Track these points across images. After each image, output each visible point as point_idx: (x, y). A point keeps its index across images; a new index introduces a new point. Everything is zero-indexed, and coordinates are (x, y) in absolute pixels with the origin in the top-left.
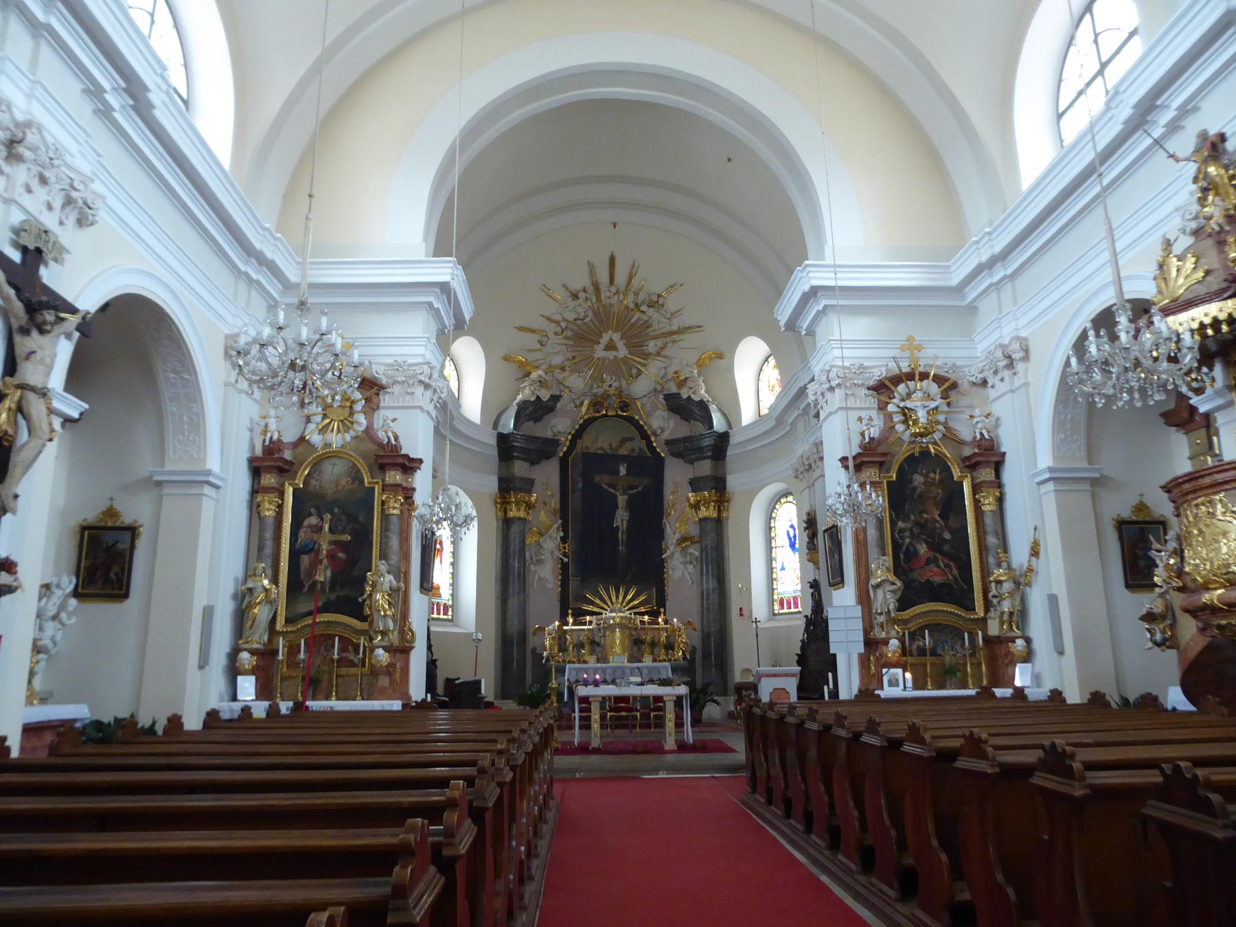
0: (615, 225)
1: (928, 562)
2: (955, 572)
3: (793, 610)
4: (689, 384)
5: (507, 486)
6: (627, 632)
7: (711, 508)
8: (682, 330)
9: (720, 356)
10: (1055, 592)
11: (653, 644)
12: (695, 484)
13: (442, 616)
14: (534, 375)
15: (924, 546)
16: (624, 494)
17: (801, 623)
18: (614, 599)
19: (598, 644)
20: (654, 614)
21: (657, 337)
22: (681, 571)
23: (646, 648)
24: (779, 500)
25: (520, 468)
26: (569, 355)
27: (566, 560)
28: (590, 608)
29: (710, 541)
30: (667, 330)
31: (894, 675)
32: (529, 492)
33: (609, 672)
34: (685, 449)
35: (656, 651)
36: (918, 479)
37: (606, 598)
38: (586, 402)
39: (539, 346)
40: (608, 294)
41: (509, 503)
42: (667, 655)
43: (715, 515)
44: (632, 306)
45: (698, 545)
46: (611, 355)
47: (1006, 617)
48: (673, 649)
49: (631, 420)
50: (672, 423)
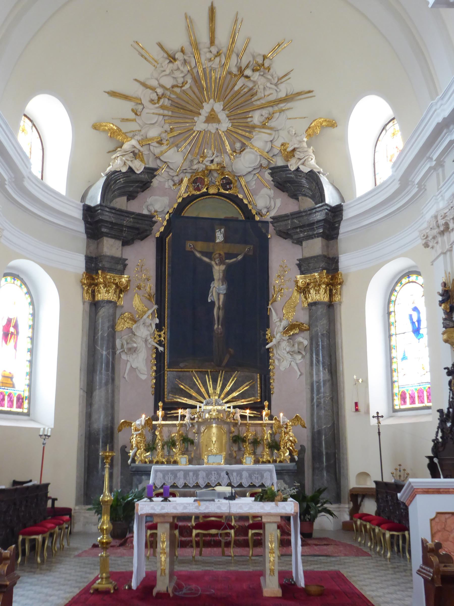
3: (417, 405)
4: (298, 155)
5: (94, 265)
6: (225, 428)
7: (322, 291)
8: (288, 99)
9: (332, 124)
11: (256, 443)
12: (304, 266)
13: (14, 409)
14: (127, 146)
17: (433, 420)
18: (211, 390)
19: (192, 442)
20: (257, 407)
21: (262, 107)
22: (288, 361)
23: (248, 447)
24: (399, 281)
25: (110, 247)
26: (167, 127)
27: (161, 349)
28: (185, 400)
29: (321, 327)
30: (273, 97)
32: (122, 272)
33: (202, 475)
34: (294, 229)
35: (259, 450)
37: (203, 390)
38: (185, 180)
39: (133, 116)
40: (209, 55)
41: (97, 285)
42: (272, 454)
43: (326, 299)
44: (235, 70)
45: (307, 334)
46: (212, 127)
48: (278, 449)
49: (234, 199)
50: (279, 202)
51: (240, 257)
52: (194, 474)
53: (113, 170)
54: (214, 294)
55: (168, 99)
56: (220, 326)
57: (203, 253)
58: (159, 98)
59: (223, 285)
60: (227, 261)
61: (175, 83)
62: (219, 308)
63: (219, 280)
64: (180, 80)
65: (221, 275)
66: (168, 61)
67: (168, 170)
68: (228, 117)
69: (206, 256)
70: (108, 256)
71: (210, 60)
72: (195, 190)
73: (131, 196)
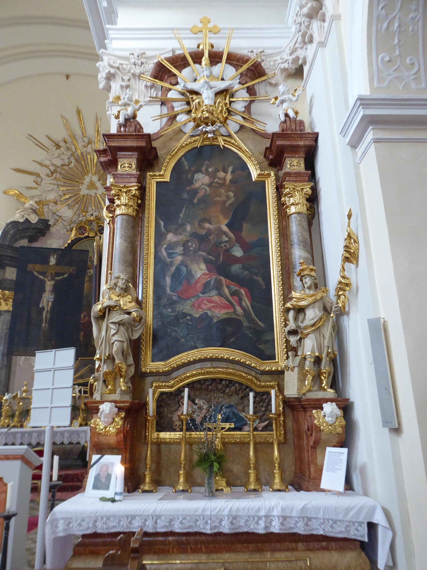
0: (68, 77)
1: (206, 288)
2: (246, 302)
10: (382, 315)
15: (203, 266)
16: (52, 279)
31: (107, 466)
36: (201, 180)
39: (35, 185)
40: (82, 144)
46: (92, 192)
47: (308, 365)
51: (66, 276)
52: (61, 435)
53: (12, 221)
54: (45, 301)
55: (60, 174)
56: (47, 325)
57: (39, 272)
58: (52, 173)
59: (51, 295)
60: (56, 278)
61: (63, 163)
62: (47, 311)
63: (49, 292)
64: (67, 161)
65: (51, 288)
66: (56, 148)
67: (62, 221)
68: (102, 185)
69: (42, 275)
70: (9, 280)
71: (85, 147)
72: (80, 234)
73: (32, 239)
